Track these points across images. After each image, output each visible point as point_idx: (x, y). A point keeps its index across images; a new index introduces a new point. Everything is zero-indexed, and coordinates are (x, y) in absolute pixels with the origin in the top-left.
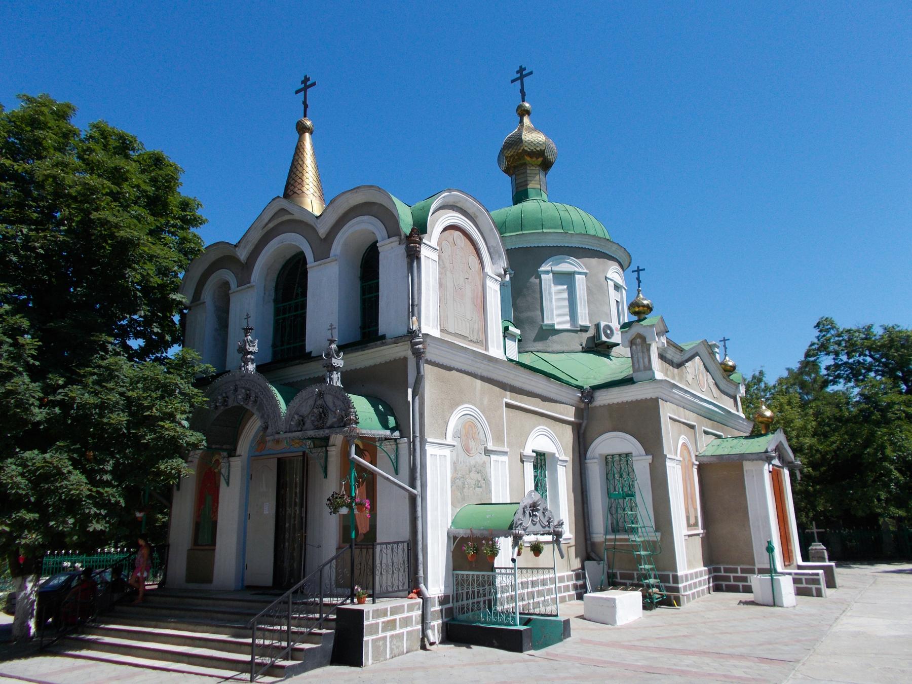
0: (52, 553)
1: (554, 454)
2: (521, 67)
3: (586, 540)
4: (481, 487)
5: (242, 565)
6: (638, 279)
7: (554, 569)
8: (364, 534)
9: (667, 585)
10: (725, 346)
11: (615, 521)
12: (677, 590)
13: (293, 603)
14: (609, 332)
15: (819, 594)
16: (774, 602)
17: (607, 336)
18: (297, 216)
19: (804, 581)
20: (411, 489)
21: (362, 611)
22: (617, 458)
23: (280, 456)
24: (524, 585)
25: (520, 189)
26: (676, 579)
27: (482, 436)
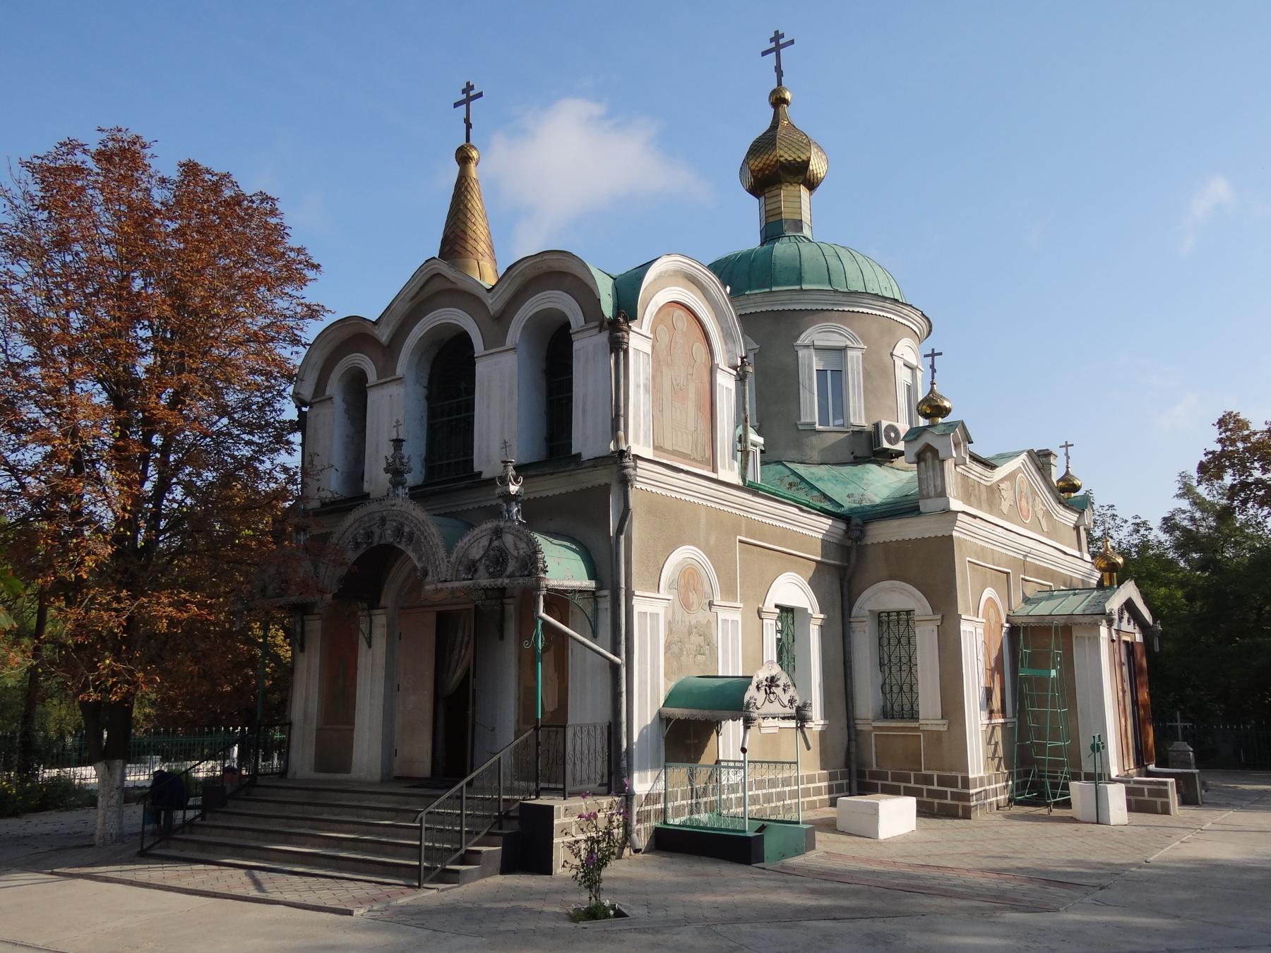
0: (210, 732)
1: (806, 609)
2: (777, 32)
3: (848, 727)
4: (704, 654)
5: (389, 750)
6: (932, 366)
7: (796, 763)
8: (552, 712)
9: (930, 787)
10: (1066, 454)
11: (889, 704)
12: (967, 797)
13: (467, 798)
14: (893, 435)
15: (1166, 810)
16: (1099, 818)
17: (890, 441)
18: (461, 285)
19: (925, 794)
20: (612, 657)
21: (553, 807)
22: (894, 617)
23: (439, 609)
24: (760, 784)
25: (771, 220)
26: (966, 782)
27: (707, 588)
